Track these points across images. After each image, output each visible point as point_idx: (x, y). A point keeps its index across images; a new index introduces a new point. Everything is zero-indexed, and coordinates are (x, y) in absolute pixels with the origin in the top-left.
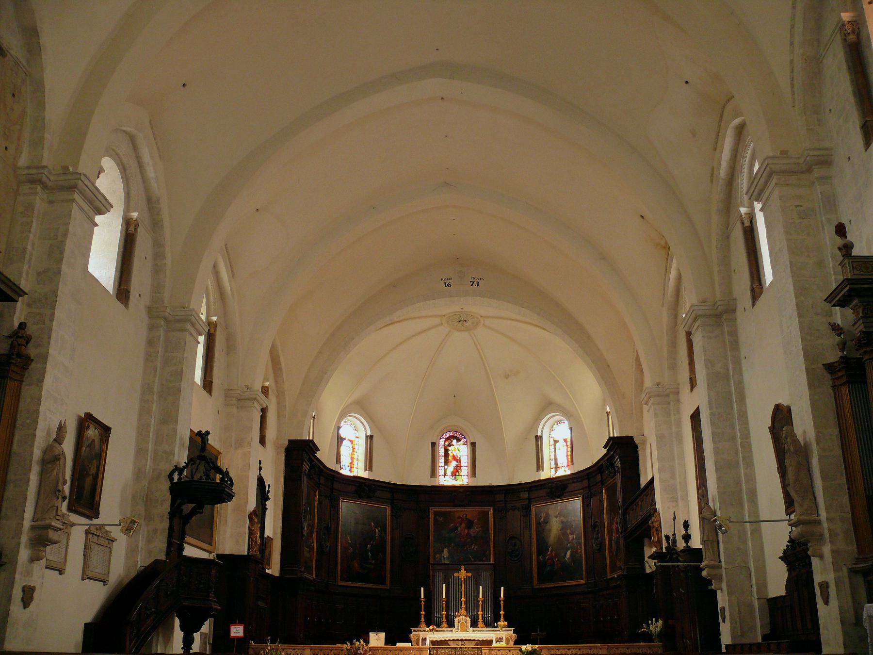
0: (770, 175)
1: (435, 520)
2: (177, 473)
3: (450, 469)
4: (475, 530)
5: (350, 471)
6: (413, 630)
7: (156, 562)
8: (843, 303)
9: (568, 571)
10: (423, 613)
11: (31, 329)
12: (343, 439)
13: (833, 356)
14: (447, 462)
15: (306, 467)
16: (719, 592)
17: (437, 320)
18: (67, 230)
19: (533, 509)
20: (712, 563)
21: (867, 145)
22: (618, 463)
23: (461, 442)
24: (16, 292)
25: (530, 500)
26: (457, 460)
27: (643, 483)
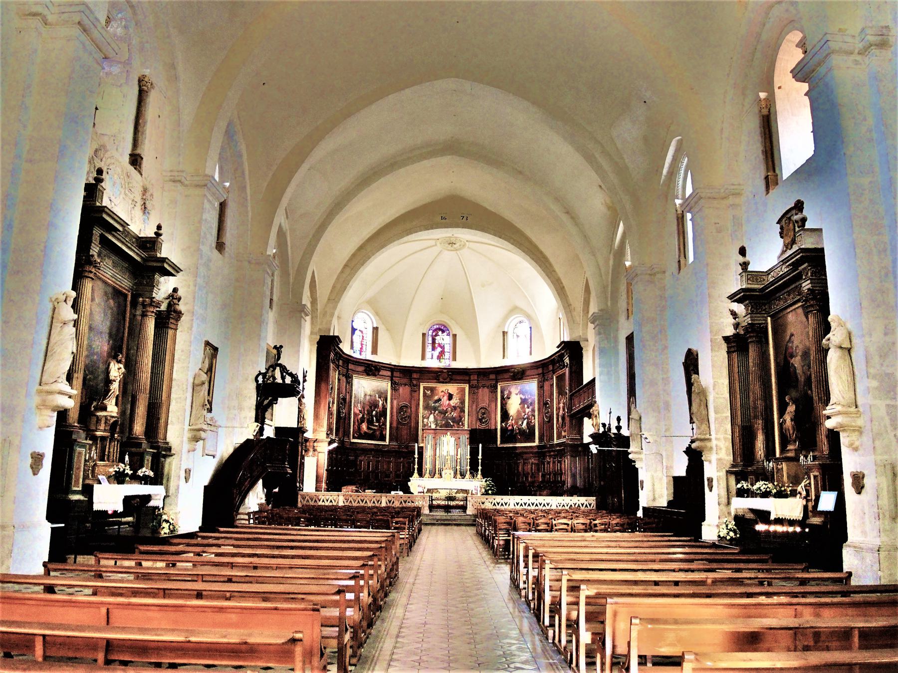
1: (424, 393)
2: (261, 377)
3: (436, 353)
4: (454, 402)
8: (739, 301)
9: (528, 435)
14: (434, 349)
15: (332, 355)
17: (433, 242)
22: (567, 360)
23: (445, 334)
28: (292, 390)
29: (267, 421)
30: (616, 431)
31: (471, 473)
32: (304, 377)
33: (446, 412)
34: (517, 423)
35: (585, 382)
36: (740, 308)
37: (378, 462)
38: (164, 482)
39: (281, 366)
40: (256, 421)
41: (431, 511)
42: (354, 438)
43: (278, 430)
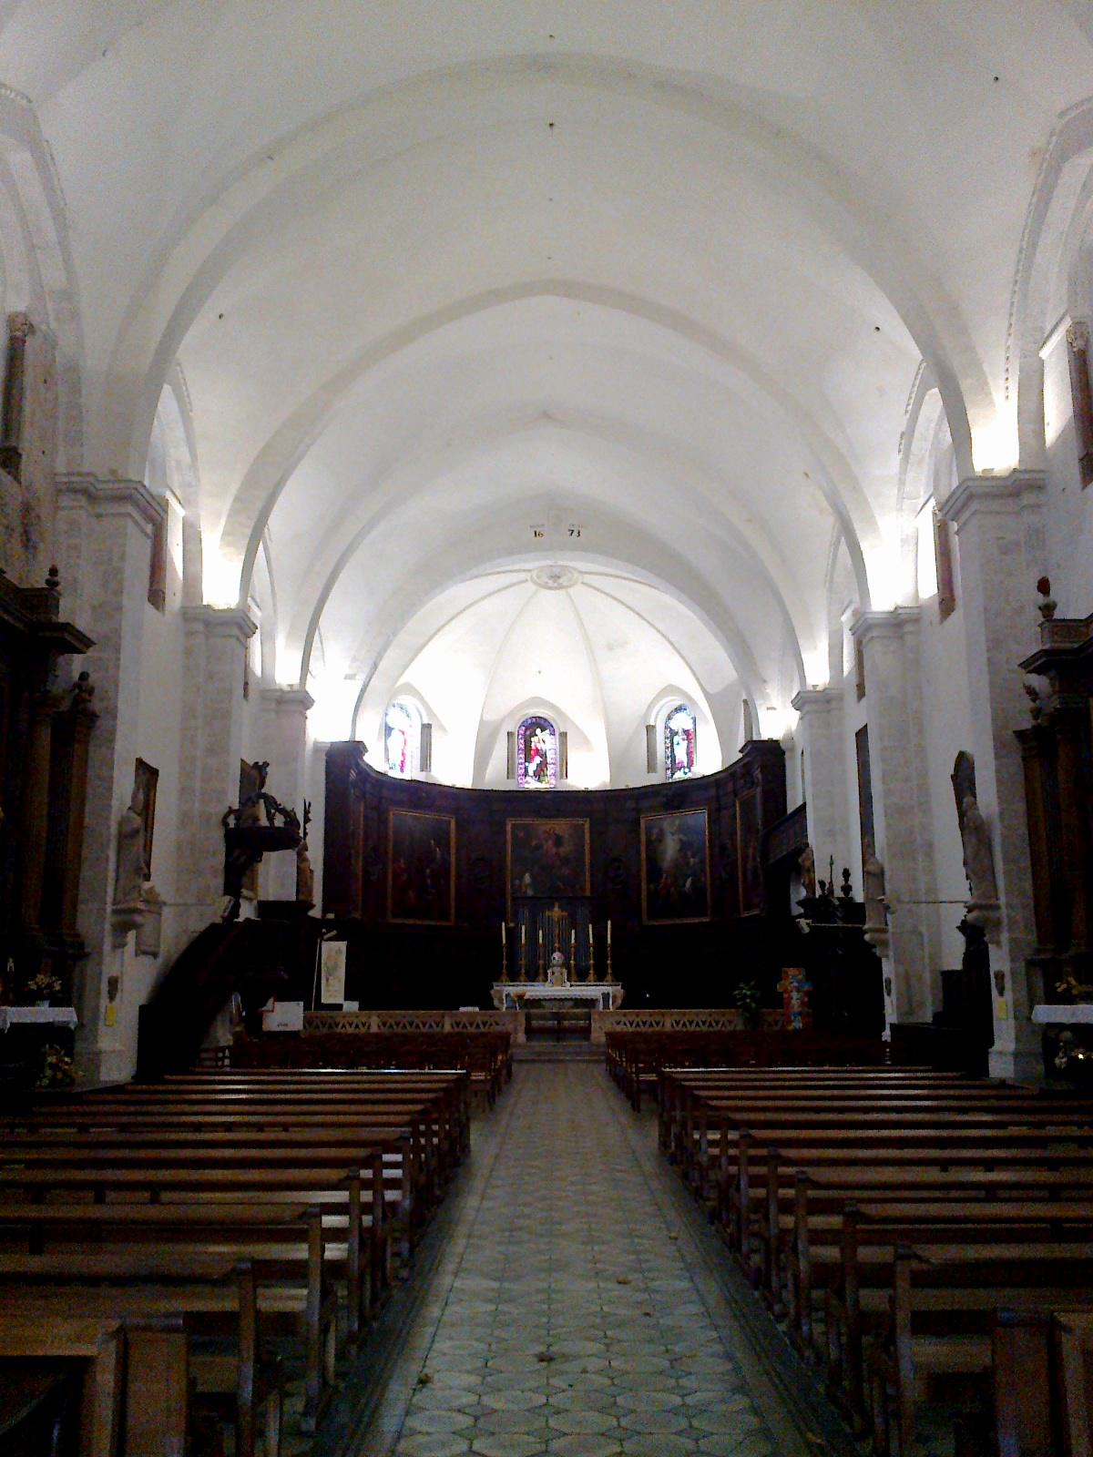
0: (970, 497)
1: (514, 836)
3: (532, 767)
5: (402, 770)
6: (494, 984)
7: (213, 926)
8: (1039, 671)
10: (505, 962)
11: (94, 678)
13: (1027, 723)
16: (884, 960)
18: (124, 553)
20: (877, 926)
21: (1085, 484)
22: (758, 774)
24: (81, 641)
25: (638, 811)
27: (791, 808)
28: (288, 837)
29: (245, 892)
30: (841, 895)
32: (307, 812)
35: (790, 809)
36: (1039, 682)
38: (75, 1000)
39: (267, 798)
40: (226, 892)
41: (529, 1039)
42: (394, 916)
43: (265, 907)
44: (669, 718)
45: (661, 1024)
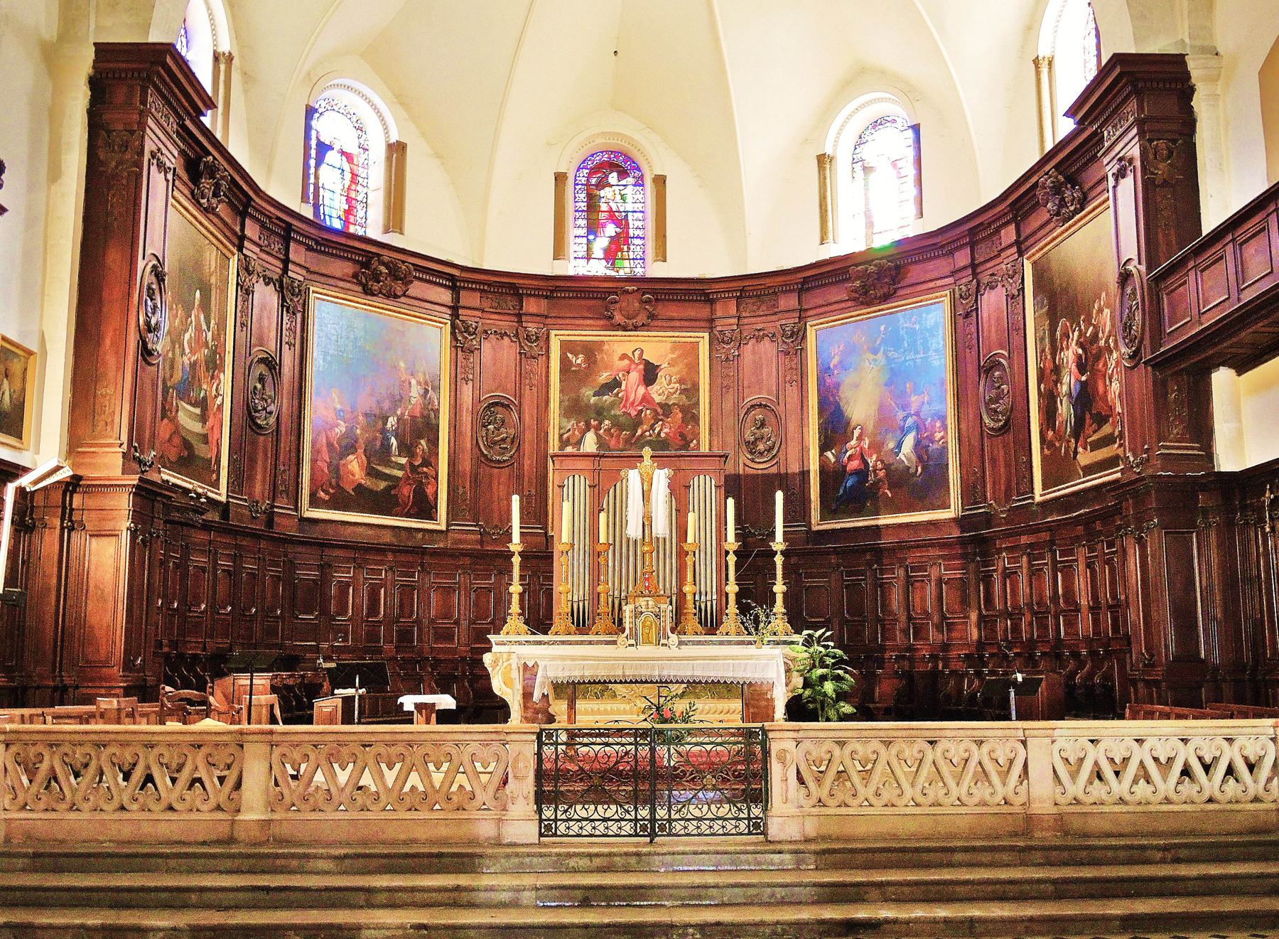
1: (565, 365)
3: (601, 244)
9: (922, 485)
12: (323, 148)
14: (593, 228)
19: (811, 334)
23: (630, 180)
25: (802, 315)
26: (618, 223)
31: (744, 609)
33: (637, 422)
34: (877, 446)
37: (407, 590)
42: (315, 502)
44: (860, 141)
45: (1017, 769)
